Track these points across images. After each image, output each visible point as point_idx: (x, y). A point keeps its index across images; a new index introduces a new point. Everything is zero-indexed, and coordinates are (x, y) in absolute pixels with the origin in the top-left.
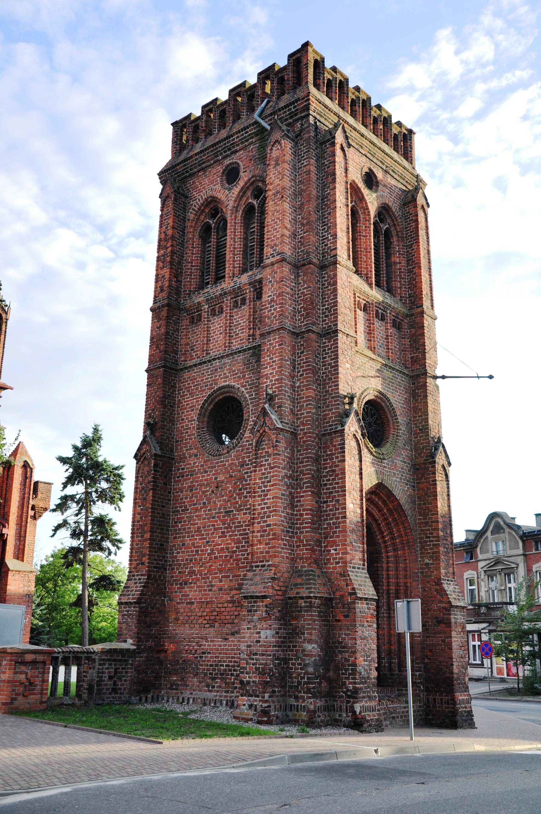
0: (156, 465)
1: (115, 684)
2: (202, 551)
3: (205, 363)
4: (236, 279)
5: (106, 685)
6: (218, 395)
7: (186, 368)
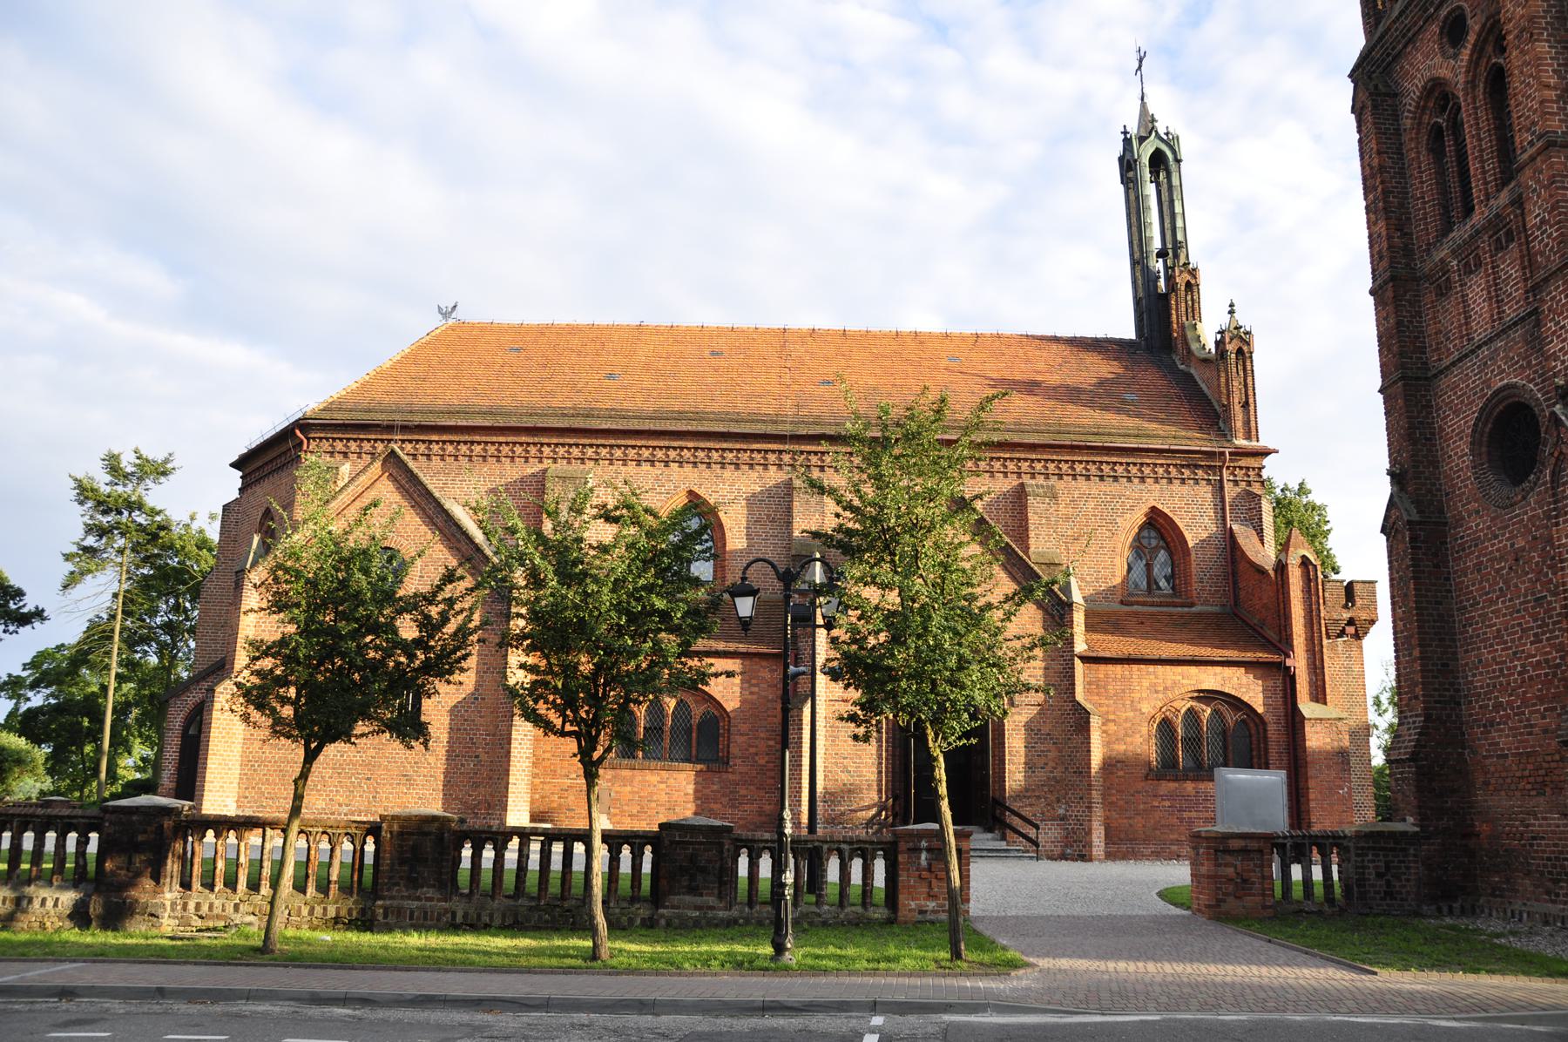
0: (1413, 539)
1: (1388, 883)
2: (1509, 669)
3: (1466, 356)
4: (1492, 202)
5: (1373, 886)
6: (1496, 405)
7: (1441, 372)
